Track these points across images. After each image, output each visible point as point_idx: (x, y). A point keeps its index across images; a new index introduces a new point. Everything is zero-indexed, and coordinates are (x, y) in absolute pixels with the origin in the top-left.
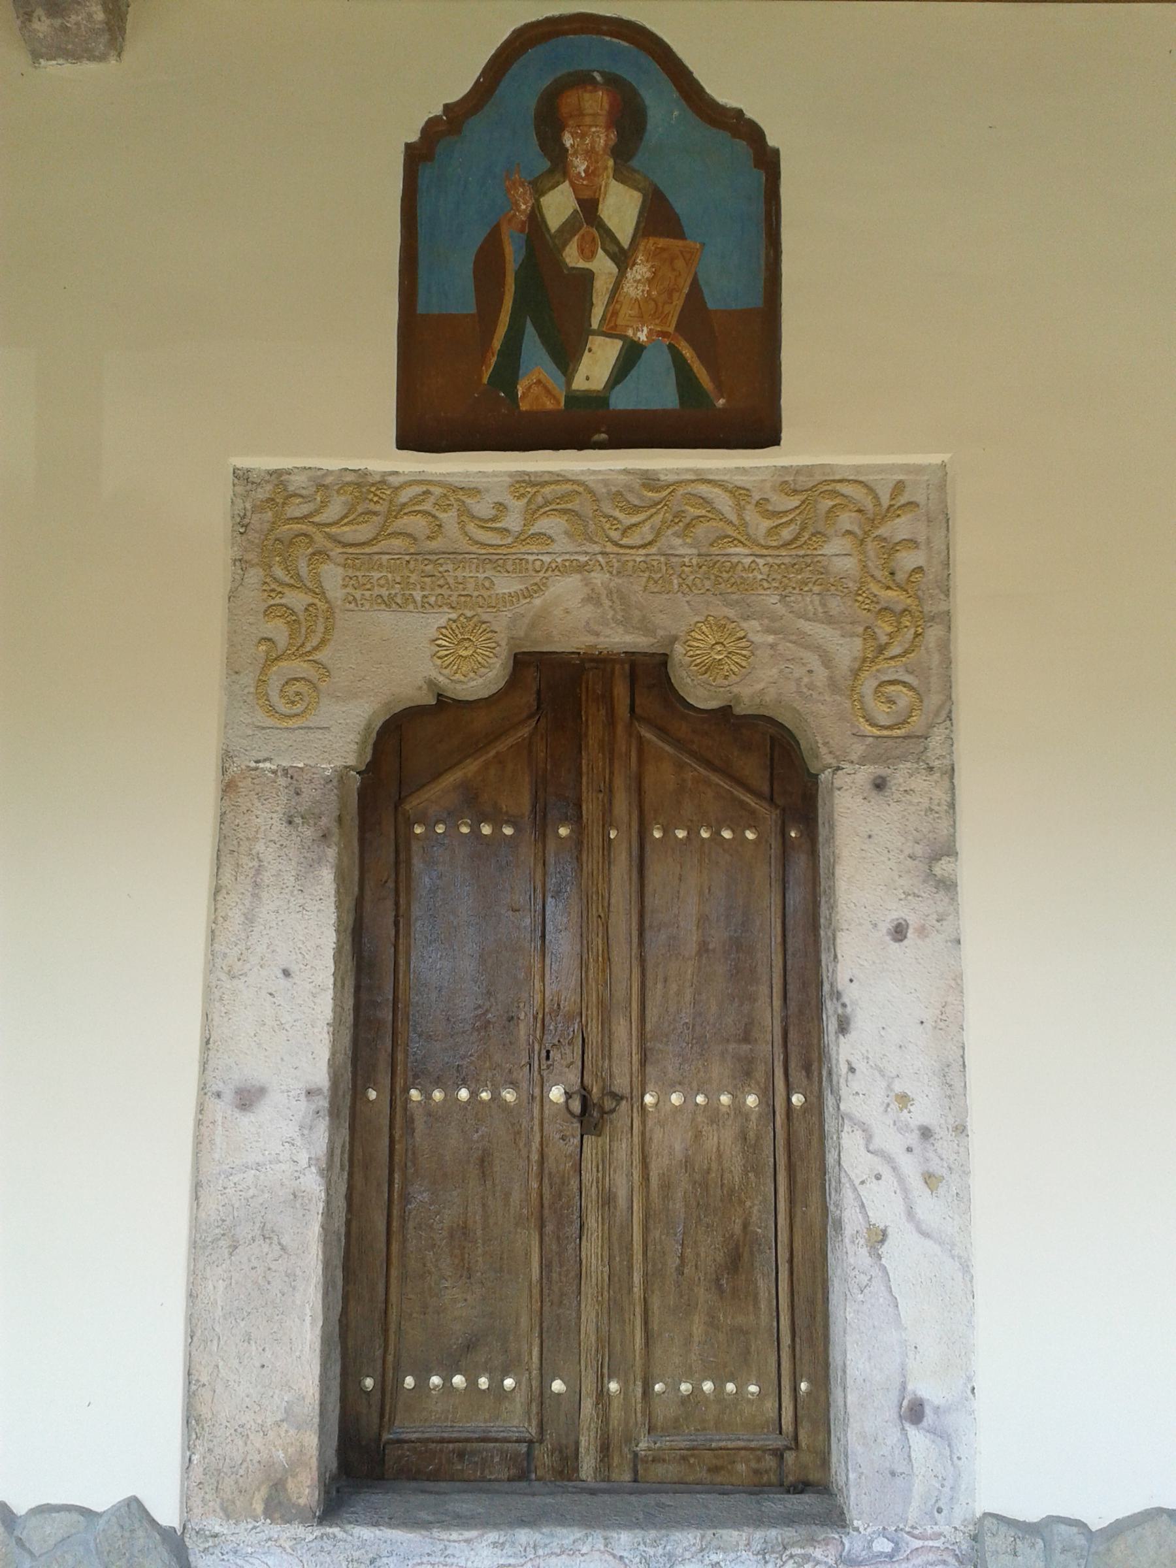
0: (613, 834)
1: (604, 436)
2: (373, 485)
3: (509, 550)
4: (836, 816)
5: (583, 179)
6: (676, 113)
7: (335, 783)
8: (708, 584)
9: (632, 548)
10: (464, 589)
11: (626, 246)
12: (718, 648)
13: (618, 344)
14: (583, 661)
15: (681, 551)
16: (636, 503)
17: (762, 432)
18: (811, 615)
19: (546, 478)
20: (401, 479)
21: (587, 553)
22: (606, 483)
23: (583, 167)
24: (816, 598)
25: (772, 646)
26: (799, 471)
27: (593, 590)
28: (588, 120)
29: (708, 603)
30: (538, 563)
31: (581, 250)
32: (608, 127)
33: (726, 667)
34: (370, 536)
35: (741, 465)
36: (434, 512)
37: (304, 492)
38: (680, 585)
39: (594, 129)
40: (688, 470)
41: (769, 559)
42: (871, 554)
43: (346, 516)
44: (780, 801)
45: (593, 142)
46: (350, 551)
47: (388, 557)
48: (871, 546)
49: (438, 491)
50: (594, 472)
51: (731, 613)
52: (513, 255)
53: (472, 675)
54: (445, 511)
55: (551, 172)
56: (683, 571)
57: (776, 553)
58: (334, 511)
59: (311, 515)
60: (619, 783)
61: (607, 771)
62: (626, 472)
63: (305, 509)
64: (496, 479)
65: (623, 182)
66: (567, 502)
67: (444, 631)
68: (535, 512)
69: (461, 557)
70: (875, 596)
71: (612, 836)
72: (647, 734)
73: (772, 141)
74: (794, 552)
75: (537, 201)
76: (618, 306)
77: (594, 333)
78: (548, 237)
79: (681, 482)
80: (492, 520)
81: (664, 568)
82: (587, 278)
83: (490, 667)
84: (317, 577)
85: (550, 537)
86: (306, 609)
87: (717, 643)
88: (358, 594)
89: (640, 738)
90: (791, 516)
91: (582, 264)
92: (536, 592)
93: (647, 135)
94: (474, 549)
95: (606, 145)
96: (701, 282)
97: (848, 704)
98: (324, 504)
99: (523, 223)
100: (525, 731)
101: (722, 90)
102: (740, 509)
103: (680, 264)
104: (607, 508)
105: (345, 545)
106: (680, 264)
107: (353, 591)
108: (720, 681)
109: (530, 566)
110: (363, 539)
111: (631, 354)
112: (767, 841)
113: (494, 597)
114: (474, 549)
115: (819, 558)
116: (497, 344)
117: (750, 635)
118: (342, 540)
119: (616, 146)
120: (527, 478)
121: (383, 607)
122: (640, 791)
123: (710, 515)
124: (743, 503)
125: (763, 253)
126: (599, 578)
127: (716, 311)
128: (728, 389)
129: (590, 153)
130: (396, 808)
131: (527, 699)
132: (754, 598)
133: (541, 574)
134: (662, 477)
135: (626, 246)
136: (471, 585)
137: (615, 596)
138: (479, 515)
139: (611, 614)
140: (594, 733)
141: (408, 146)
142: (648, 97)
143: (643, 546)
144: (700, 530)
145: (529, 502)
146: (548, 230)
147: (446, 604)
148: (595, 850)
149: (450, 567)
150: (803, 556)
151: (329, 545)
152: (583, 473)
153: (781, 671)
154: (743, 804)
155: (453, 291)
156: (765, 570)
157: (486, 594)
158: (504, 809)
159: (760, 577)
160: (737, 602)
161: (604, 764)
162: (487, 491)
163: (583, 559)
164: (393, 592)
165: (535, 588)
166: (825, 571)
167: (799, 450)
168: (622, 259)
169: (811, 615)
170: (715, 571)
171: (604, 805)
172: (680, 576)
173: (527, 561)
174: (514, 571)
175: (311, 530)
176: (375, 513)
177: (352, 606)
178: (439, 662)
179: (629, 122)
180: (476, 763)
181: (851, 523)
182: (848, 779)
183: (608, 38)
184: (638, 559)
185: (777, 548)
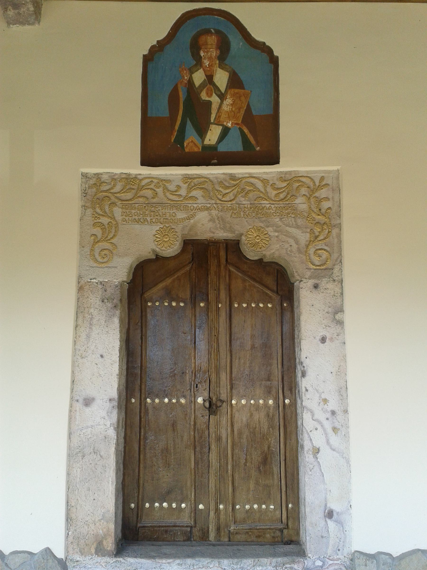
1: (216, 161)
2: (132, 178)
3: (182, 202)
4: (300, 298)
5: (208, 68)
6: (241, 44)
7: (119, 287)
8: (254, 214)
11: (223, 92)
12: (258, 237)
13: (221, 128)
15: (244, 203)
16: (228, 185)
17: (273, 159)
19: (195, 176)
20: (143, 177)
21: (210, 203)
22: (217, 178)
23: (208, 63)
25: (277, 237)
26: (286, 173)
27: (212, 217)
30: (192, 207)
31: (207, 94)
32: (216, 50)
34: (131, 197)
37: (107, 181)
38: (244, 215)
39: (211, 50)
40: (246, 173)
43: (122, 190)
45: (211, 54)
46: (124, 202)
48: (312, 200)
51: (262, 225)
52: (182, 96)
53: (168, 248)
54: (158, 188)
55: (196, 65)
56: (245, 210)
57: (278, 203)
58: (118, 188)
59: (110, 189)
60: (222, 287)
61: (218, 283)
62: (224, 174)
63: (107, 187)
65: (222, 69)
67: (158, 232)
69: (164, 205)
70: (314, 218)
72: (232, 269)
73: (275, 54)
74: (285, 203)
75: (191, 76)
76: (220, 114)
79: (244, 177)
80: (176, 191)
87: (257, 236)
88: (127, 218)
89: (229, 271)
90: (283, 190)
91: (207, 99)
92: (191, 217)
94: (169, 202)
96: (251, 105)
97: (304, 257)
98: (114, 185)
99: (186, 84)
100: (188, 268)
101: (258, 36)
102: (265, 187)
103: (243, 98)
104: (217, 187)
106: (243, 98)
108: (258, 249)
109: (189, 208)
110: (128, 198)
112: (276, 307)
114: (169, 202)
115: (294, 205)
116: (177, 128)
117: (269, 233)
118: (120, 198)
120: (188, 176)
121: (136, 223)
122: (230, 290)
124: (266, 185)
125: (273, 94)
129: (210, 58)
132: (270, 219)
133: (193, 211)
134: (237, 176)
136: (168, 215)
137: (220, 219)
138: (171, 190)
140: (213, 269)
141: (144, 56)
142: (231, 38)
143: (231, 201)
144: (251, 195)
146: (195, 86)
147: (159, 222)
150: (288, 204)
151: (117, 201)
155: (160, 109)
157: (173, 218)
159: (273, 212)
160: (264, 221)
162: (174, 181)
163: (209, 205)
165: (191, 216)
166: (296, 209)
167: (286, 165)
168: (222, 97)
170: (256, 210)
171: (216, 295)
173: (188, 207)
174: (183, 210)
175: (110, 195)
176: (133, 189)
177: (125, 223)
178: (156, 243)
179: (224, 47)
181: (305, 192)
182: (305, 285)
183: (216, 17)
184: (229, 206)
185: (279, 201)
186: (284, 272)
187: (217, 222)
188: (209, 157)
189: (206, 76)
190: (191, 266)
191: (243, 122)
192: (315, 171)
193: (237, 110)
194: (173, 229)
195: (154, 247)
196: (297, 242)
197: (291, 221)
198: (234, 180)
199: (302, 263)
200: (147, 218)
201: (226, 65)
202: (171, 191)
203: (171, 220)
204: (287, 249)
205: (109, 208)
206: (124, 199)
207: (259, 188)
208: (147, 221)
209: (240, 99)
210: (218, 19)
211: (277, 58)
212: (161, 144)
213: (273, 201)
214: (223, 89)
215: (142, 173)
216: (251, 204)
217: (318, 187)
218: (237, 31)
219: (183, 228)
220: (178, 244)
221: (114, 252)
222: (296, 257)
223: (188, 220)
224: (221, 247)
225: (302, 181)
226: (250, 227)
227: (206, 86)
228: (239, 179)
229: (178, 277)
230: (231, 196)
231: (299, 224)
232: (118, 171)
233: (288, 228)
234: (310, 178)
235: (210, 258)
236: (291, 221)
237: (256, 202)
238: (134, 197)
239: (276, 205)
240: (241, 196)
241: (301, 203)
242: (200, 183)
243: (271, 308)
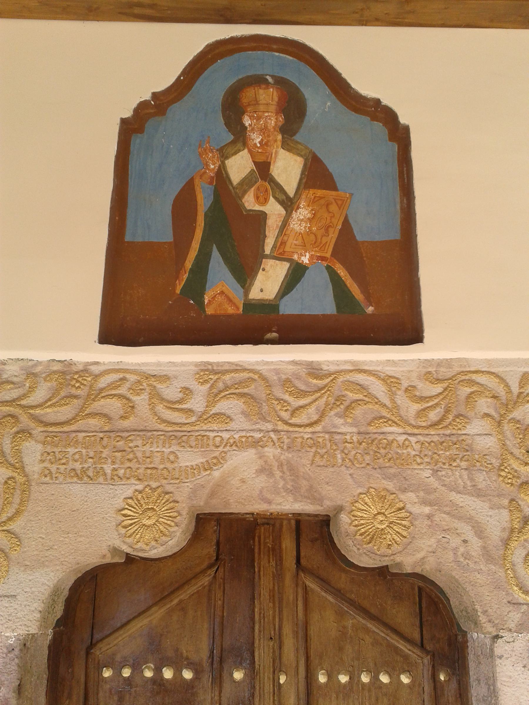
0: (283, 679)
1: (275, 335)
2: (77, 373)
3: (193, 428)
4: (499, 685)
5: (259, 148)
6: (329, 104)
7: (17, 652)
8: (367, 458)
9: (300, 426)
10: (151, 463)
11: (292, 195)
12: (380, 517)
13: (287, 265)
14: (256, 520)
15: (343, 429)
16: (303, 388)
17: (409, 332)
18: (461, 488)
19: (226, 367)
20: (102, 368)
21: (260, 431)
22: (277, 372)
23: (259, 140)
24: (465, 473)
25: (429, 517)
26: (440, 363)
27: (266, 462)
28: (262, 108)
29: (369, 477)
30: (218, 439)
31: (257, 198)
32: (277, 113)
33: (389, 537)
34: (70, 416)
35: (391, 359)
36: (129, 395)
37: (15, 379)
38: (343, 460)
39: (266, 114)
40: (346, 362)
41: (419, 437)
42: (508, 434)
43: (49, 400)
44: (429, 647)
45: (266, 123)
46: (51, 429)
47: (84, 434)
48: (507, 427)
49: (133, 378)
50: (267, 363)
51: (390, 485)
52: (204, 200)
53: (153, 543)
54: (138, 394)
55: (233, 142)
56: (345, 447)
57: (426, 432)
58: (40, 394)
59: (19, 398)
60: (287, 630)
61: (277, 620)
62: (294, 363)
63: (15, 394)
64: (183, 368)
65: (289, 150)
66: (244, 387)
67: (130, 501)
68: (216, 395)
69: (150, 434)
70: (516, 471)
71: (282, 681)
72: (312, 584)
73: (403, 120)
74: (441, 432)
75: (223, 163)
76: (285, 238)
77: (267, 257)
78: (231, 187)
79: (341, 371)
80: (180, 402)
81: (329, 445)
82: (262, 217)
83: (171, 536)
84: (18, 453)
85: (229, 417)
86: (6, 482)
87: (379, 513)
88: (54, 468)
89: (306, 589)
90: (436, 401)
91: (257, 208)
92: (215, 464)
93: (307, 118)
94: (162, 427)
95: (276, 125)
96: (351, 221)
97: (501, 573)
98: (32, 389)
99: (212, 178)
100: (205, 580)
101: (364, 86)
102: (392, 395)
103: (334, 208)
104: (278, 392)
105: (47, 424)
106: (334, 208)
107: (49, 465)
108: (384, 550)
109: (211, 442)
110: (63, 419)
111: (296, 274)
112: (420, 685)
113: (177, 470)
114: (162, 427)
115: (464, 437)
116: (189, 264)
117: (408, 506)
118: (44, 419)
119: (283, 125)
120: (210, 367)
121: (75, 479)
122: (306, 638)
123: (366, 399)
124: (394, 389)
125: (398, 200)
126: (270, 452)
127: (363, 242)
128: (380, 299)
129: (264, 130)
130: (88, 653)
131: (209, 550)
132: (409, 472)
133: (221, 449)
134: (325, 367)
135: (292, 195)
136: (157, 460)
137: (285, 468)
138: (168, 398)
139: (281, 484)
140: (265, 584)
141: (124, 121)
142: (307, 93)
143: (311, 425)
144: (358, 411)
145: (212, 387)
146: (231, 183)
147: (134, 476)
148: (266, 696)
149: (139, 443)
150: (450, 435)
151: (32, 425)
152: (258, 363)
153: (439, 541)
154: (397, 650)
155: (154, 224)
156: (417, 447)
157: (170, 466)
158: (185, 654)
159: (414, 453)
160: (395, 475)
161: (274, 612)
162: (176, 377)
163: (258, 435)
164: (86, 466)
165: (215, 461)
166: (469, 449)
167: (437, 347)
168: (289, 204)
169: (461, 488)
170: (374, 448)
171: (274, 652)
172: (343, 451)
173: (208, 437)
174: (196, 446)
175: (17, 411)
176: (76, 397)
177: (48, 479)
178: (123, 531)
179: (293, 110)
180: (162, 610)
181: (488, 407)
182: (507, 647)
183: (277, 54)
184: (306, 436)
185: (427, 427)
186: (439, 598)
187: (278, 474)
188: (257, 326)
189: (255, 163)
190: (213, 574)
191: (334, 254)
192: (507, 360)
193: (323, 230)
194: (167, 493)
195: (118, 543)
196: (480, 533)
197: (461, 476)
198: (317, 377)
199: (498, 587)
200: (105, 466)
201: (297, 142)
202: (169, 402)
203: (165, 472)
204: (455, 549)
205: (12, 443)
206: (52, 421)
207: (378, 396)
208: (105, 474)
209: (328, 210)
210: (279, 57)
211: (407, 129)
212: (151, 296)
213: (414, 426)
214: (291, 189)
215: (101, 361)
216: (359, 433)
217: (518, 397)
218: (319, 80)
219: (194, 491)
220: (178, 534)
221: (13, 555)
222: (480, 571)
223: (206, 470)
224: (284, 527)
225: (478, 383)
226: (360, 490)
227: (256, 182)
228: (330, 375)
229: (181, 602)
230: (312, 414)
231: (482, 485)
232: (42, 356)
233: (454, 496)
234: (497, 376)
235: (259, 553)
236: (461, 476)
237: (371, 429)
238: (77, 415)
239: (421, 438)
240: (336, 415)
241: (479, 433)
242: (240, 383)
243: (409, 686)
